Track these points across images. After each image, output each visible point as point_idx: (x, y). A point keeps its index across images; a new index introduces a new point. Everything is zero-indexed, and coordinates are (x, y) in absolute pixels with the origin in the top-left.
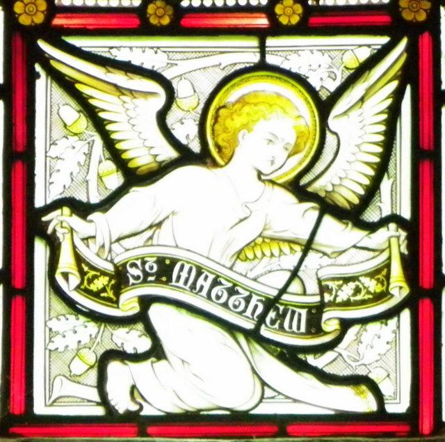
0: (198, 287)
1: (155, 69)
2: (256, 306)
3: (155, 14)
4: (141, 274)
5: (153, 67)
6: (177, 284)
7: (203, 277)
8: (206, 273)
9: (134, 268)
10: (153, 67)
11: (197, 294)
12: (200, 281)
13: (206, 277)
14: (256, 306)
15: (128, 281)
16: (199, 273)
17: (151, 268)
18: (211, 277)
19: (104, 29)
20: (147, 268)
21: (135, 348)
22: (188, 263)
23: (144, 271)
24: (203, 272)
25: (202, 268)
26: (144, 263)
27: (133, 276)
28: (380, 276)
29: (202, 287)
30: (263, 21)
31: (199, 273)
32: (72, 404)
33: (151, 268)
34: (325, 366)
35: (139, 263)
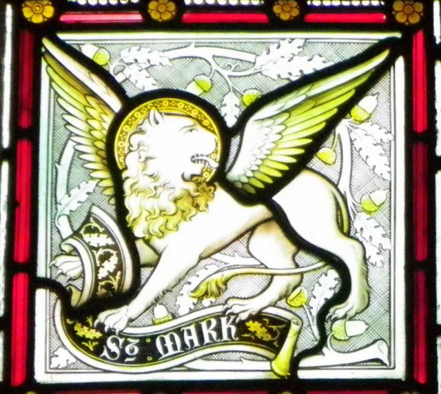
0: (188, 343)
1: (238, 116)
2: (229, 330)
3: (289, 12)
4: (118, 352)
5: (236, 116)
6: (167, 355)
7: (185, 334)
8: (185, 329)
9: (114, 344)
10: (236, 116)
11: (191, 349)
12: (187, 338)
13: (189, 333)
14: (229, 330)
15: (102, 351)
16: (181, 335)
17: (132, 351)
18: (192, 328)
19: (372, 24)
20: (127, 350)
21: (226, 114)
22: (166, 334)
23: (123, 351)
24: (183, 330)
25: (180, 328)
26: (126, 343)
27: (109, 350)
28: (274, 327)
29: (192, 342)
30: (137, 17)
31: (181, 335)
32: (393, 210)
33: (132, 351)
34: (71, 226)
35: (121, 341)
